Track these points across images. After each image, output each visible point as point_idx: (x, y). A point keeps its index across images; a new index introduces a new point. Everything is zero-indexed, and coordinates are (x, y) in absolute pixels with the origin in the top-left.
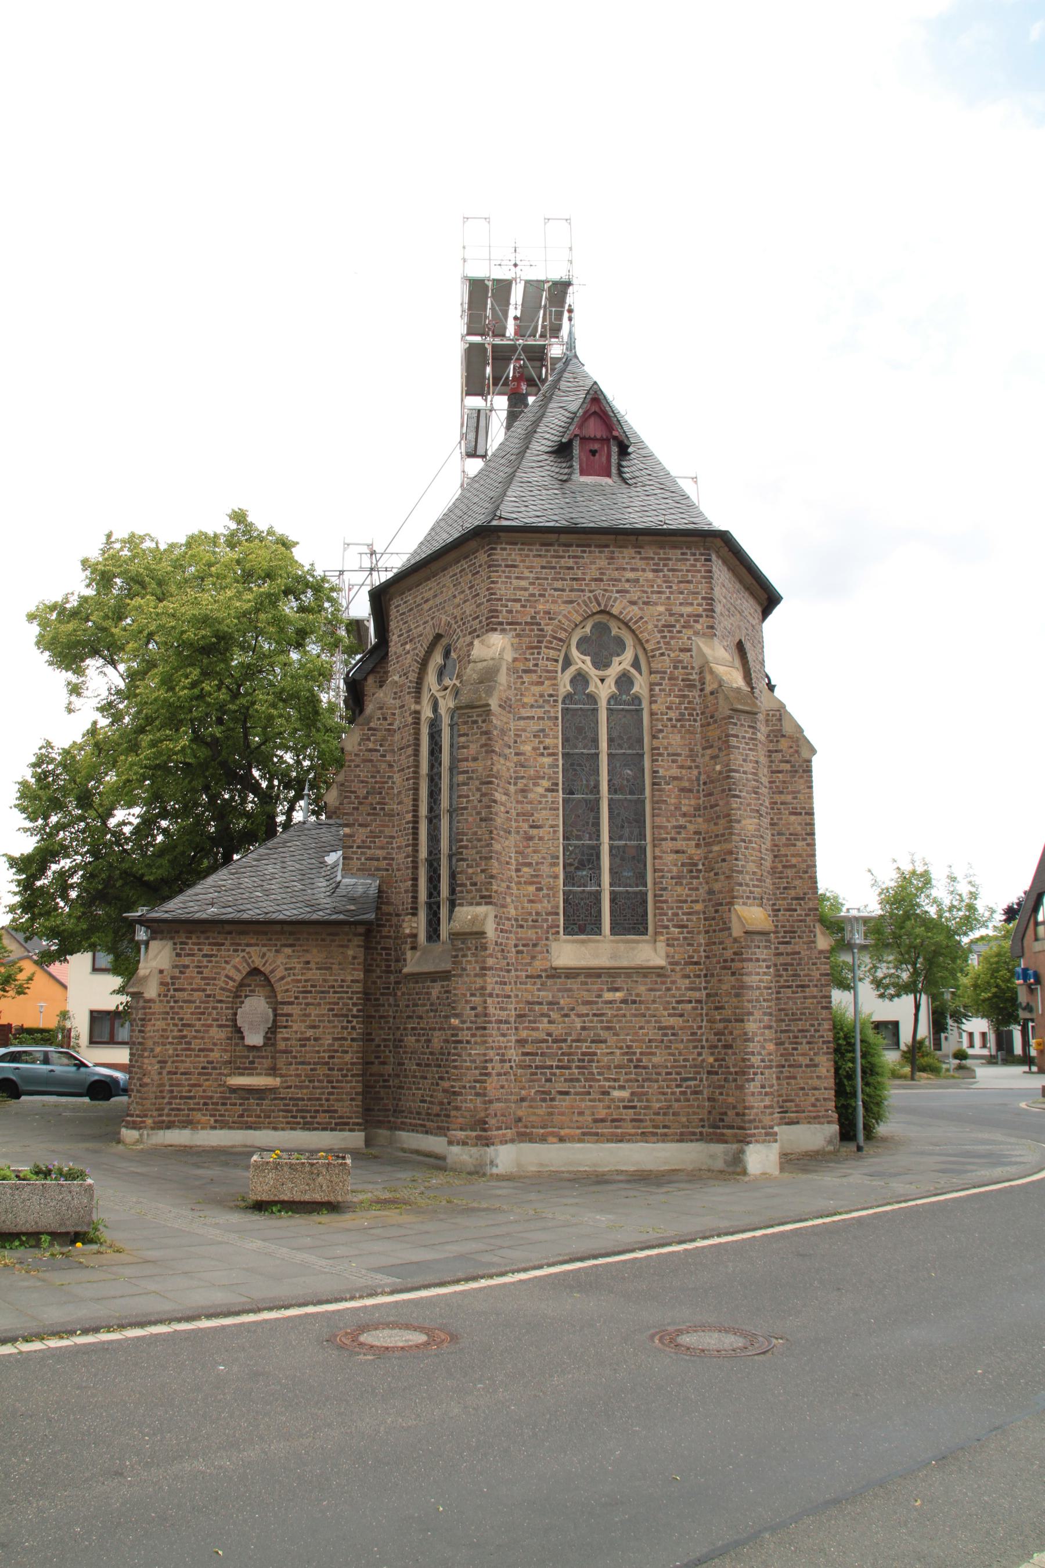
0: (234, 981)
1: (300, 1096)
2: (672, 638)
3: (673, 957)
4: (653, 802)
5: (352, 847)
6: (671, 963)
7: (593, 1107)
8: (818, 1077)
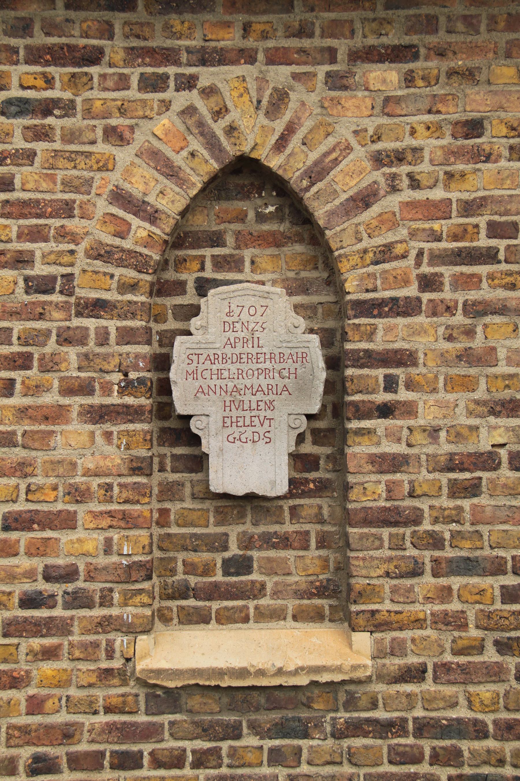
0: (153, 217)
1: (462, 712)
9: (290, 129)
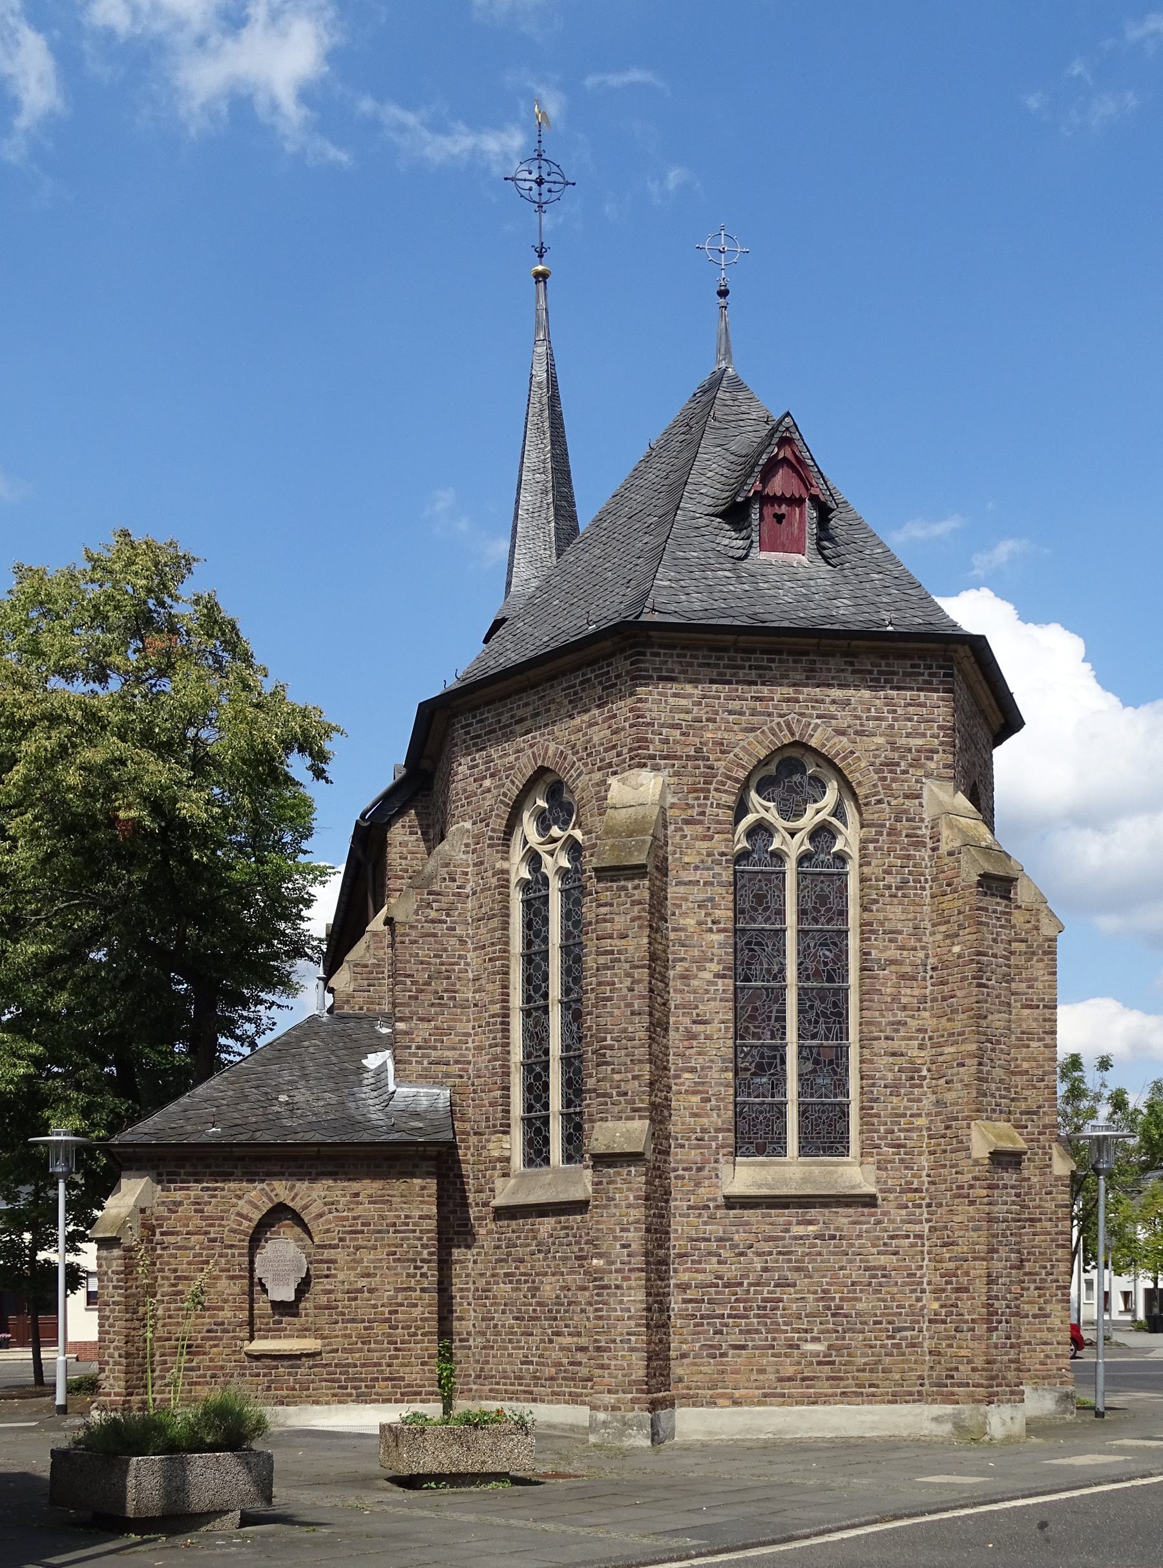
0: (250, 1220)
1: (350, 1361)
2: (893, 780)
3: (886, 1182)
4: (862, 993)
5: (410, 1047)
6: (881, 1191)
7: (776, 1364)
8: (1050, 1330)
9: (296, 1195)
